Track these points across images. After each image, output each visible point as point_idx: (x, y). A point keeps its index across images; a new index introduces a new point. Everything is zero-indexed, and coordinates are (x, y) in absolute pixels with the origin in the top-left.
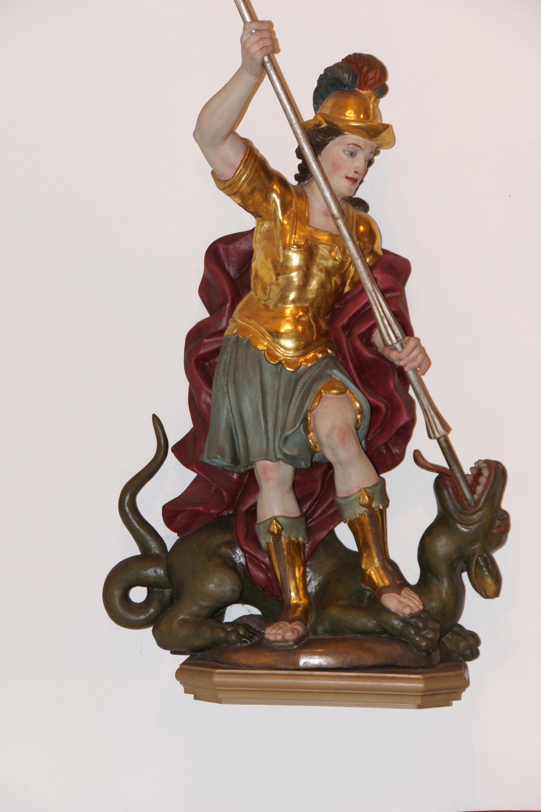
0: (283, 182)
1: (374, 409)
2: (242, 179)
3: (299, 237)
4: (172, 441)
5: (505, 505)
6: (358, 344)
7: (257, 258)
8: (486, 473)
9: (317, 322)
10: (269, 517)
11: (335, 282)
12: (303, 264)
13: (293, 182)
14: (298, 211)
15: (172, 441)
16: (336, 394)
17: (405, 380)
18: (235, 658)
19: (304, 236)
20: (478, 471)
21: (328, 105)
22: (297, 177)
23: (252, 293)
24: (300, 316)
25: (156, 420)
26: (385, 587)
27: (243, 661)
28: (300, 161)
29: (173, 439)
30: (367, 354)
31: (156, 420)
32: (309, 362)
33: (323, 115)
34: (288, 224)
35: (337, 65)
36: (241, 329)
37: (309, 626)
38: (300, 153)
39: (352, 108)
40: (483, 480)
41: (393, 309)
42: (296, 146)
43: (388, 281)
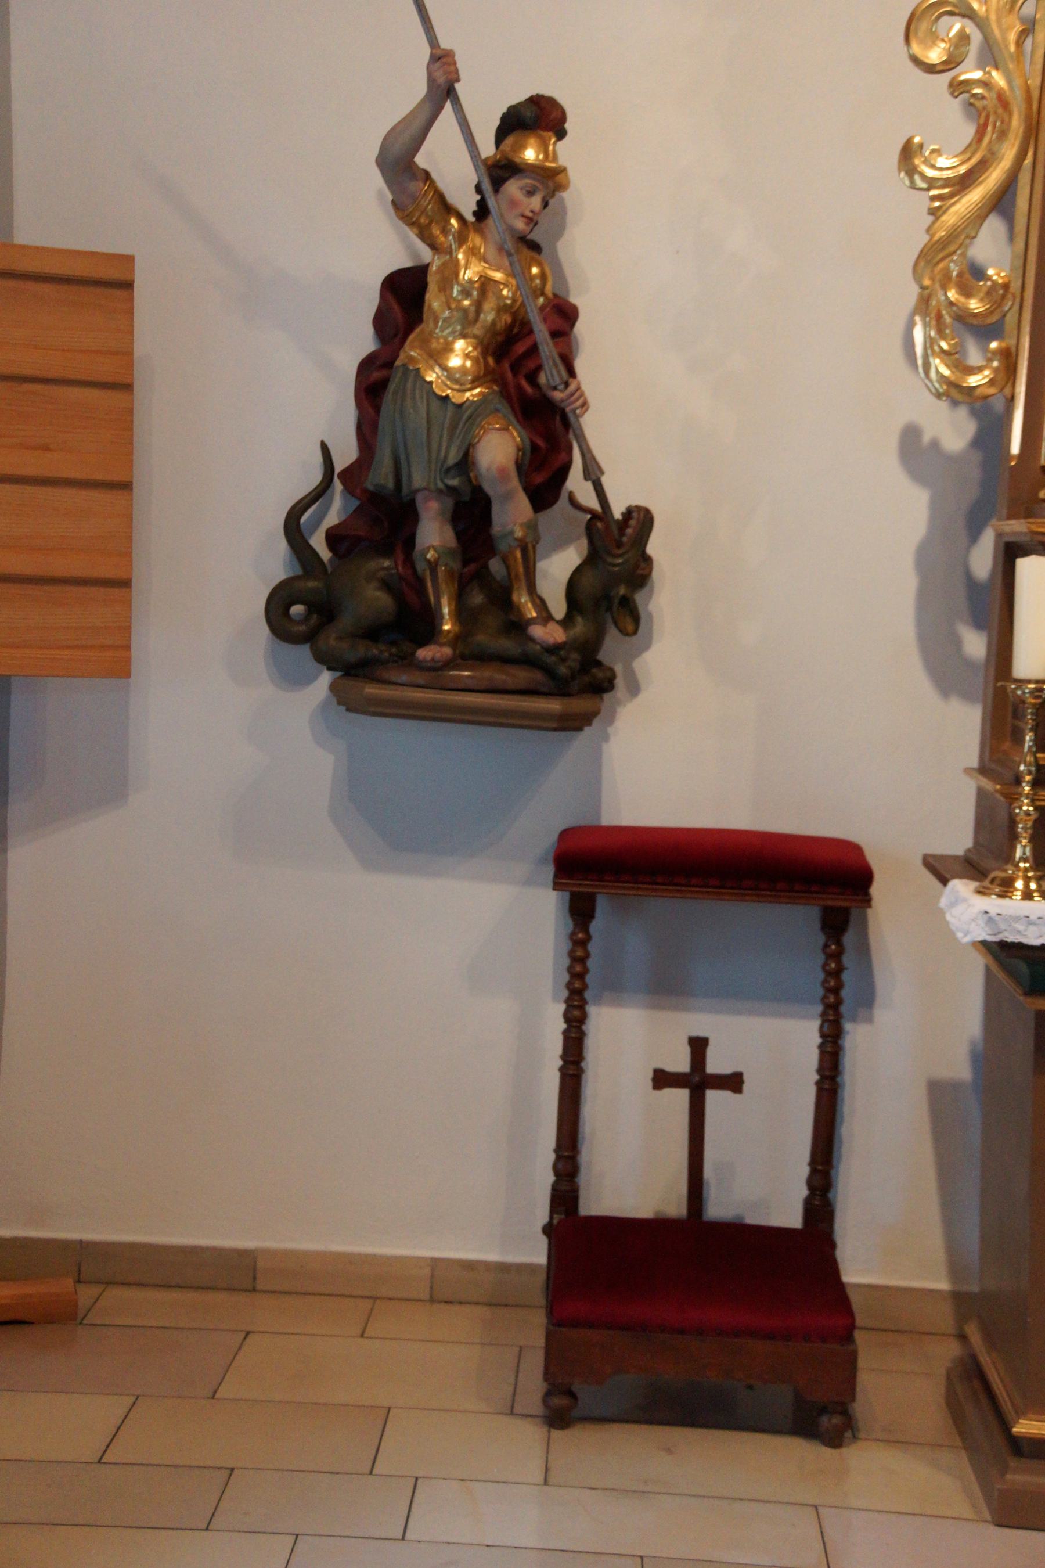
0: (460, 218)
1: (534, 447)
2: (314, 512)
3: (474, 272)
4: (339, 467)
5: (651, 549)
6: (524, 383)
7: (430, 292)
8: (635, 515)
9: (485, 359)
10: (427, 545)
11: (505, 320)
12: (577, 417)
13: (471, 218)
14: (936, 389)
15: (339, 467)
16: (499, 430)
17: (566, 424)
18: (386, 675)
19: (478, 272)
20: (629, 513)
21: (509, 141)
22: (475, 214)
23: (423, 325)
24: (470, 352)
25: (325, 448)
26: (533, 619)
27: (394, 679)
28: (478, 197)
29: (339, 466)
30: (529, 389)
31: (325, 448)
32: (476, 397)
33: (502, 152)
34: (463, 259)
35: (520, 104)
36: (412, 359)
37: (458, 652)
38: (478, 189)
39: (532, 147)
40: (632, 522)
41: (429, 242)
42: (475, 181)
43: (558, 323)
